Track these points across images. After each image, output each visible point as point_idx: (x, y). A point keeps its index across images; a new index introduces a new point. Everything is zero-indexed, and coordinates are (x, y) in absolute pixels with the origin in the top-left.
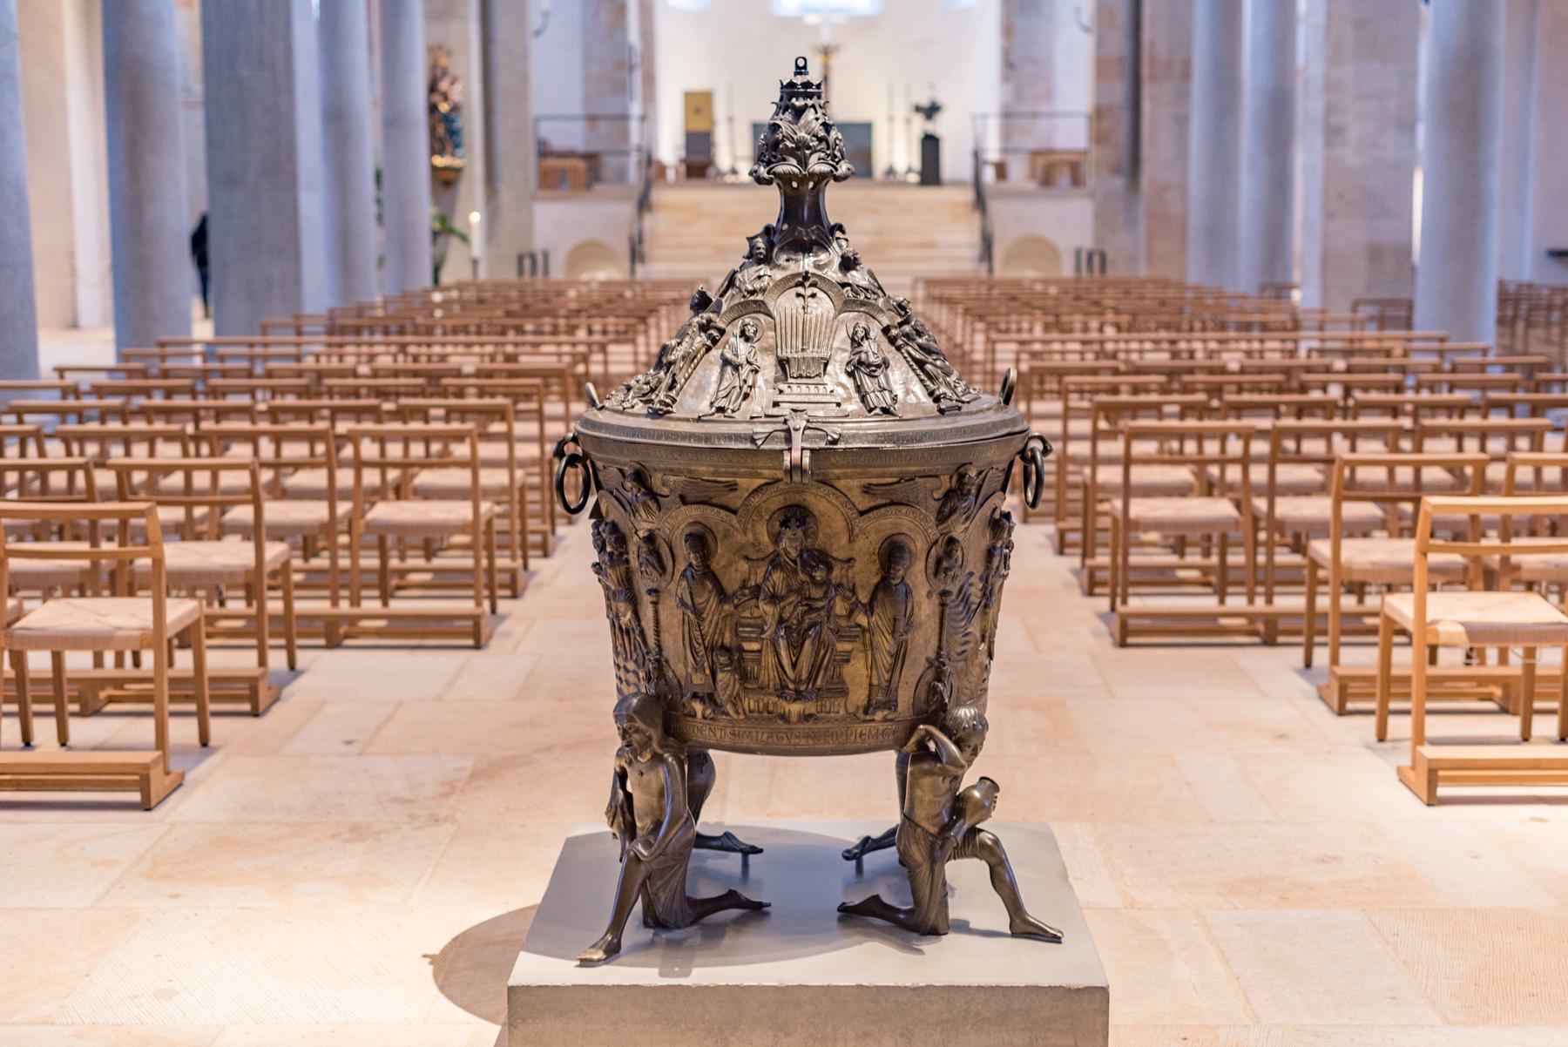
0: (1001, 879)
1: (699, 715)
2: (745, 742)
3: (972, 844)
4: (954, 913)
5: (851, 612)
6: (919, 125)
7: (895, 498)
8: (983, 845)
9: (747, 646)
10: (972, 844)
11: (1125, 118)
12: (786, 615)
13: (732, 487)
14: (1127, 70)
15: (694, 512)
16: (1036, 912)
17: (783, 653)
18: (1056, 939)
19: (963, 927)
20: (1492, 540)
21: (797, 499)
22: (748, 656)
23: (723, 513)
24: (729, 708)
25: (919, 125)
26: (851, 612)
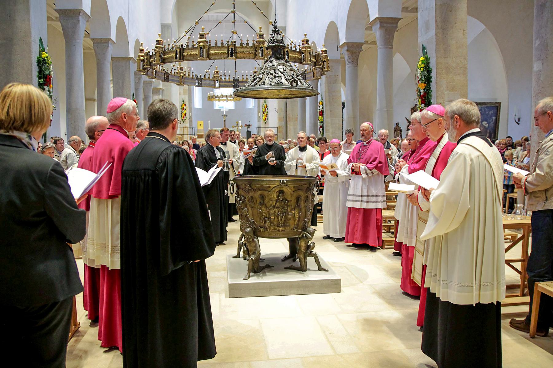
0: (317, 261)
1: (262, 231)
2: (279, 236)
3: (311, 254)
4: (308, 267)
5: (291, 210)
6: (246, 129)
7: (299, 189)
8: (313, 254)
9: (271, 217)
10: (311, 254)
11: (285, 127)
12: (279, 211)
13: (269, 187)
14: (285, 119)
15: (260, 192)
16: (323, 266)
17: (279, 218)
18: (327, 271)
19: (309, 270)
20: (286, 209)
21: (282, 189)
22: (272, 219)
23: (267, 192)
24: (268, 229)
25: (246, 129)
26: (291, 210)
